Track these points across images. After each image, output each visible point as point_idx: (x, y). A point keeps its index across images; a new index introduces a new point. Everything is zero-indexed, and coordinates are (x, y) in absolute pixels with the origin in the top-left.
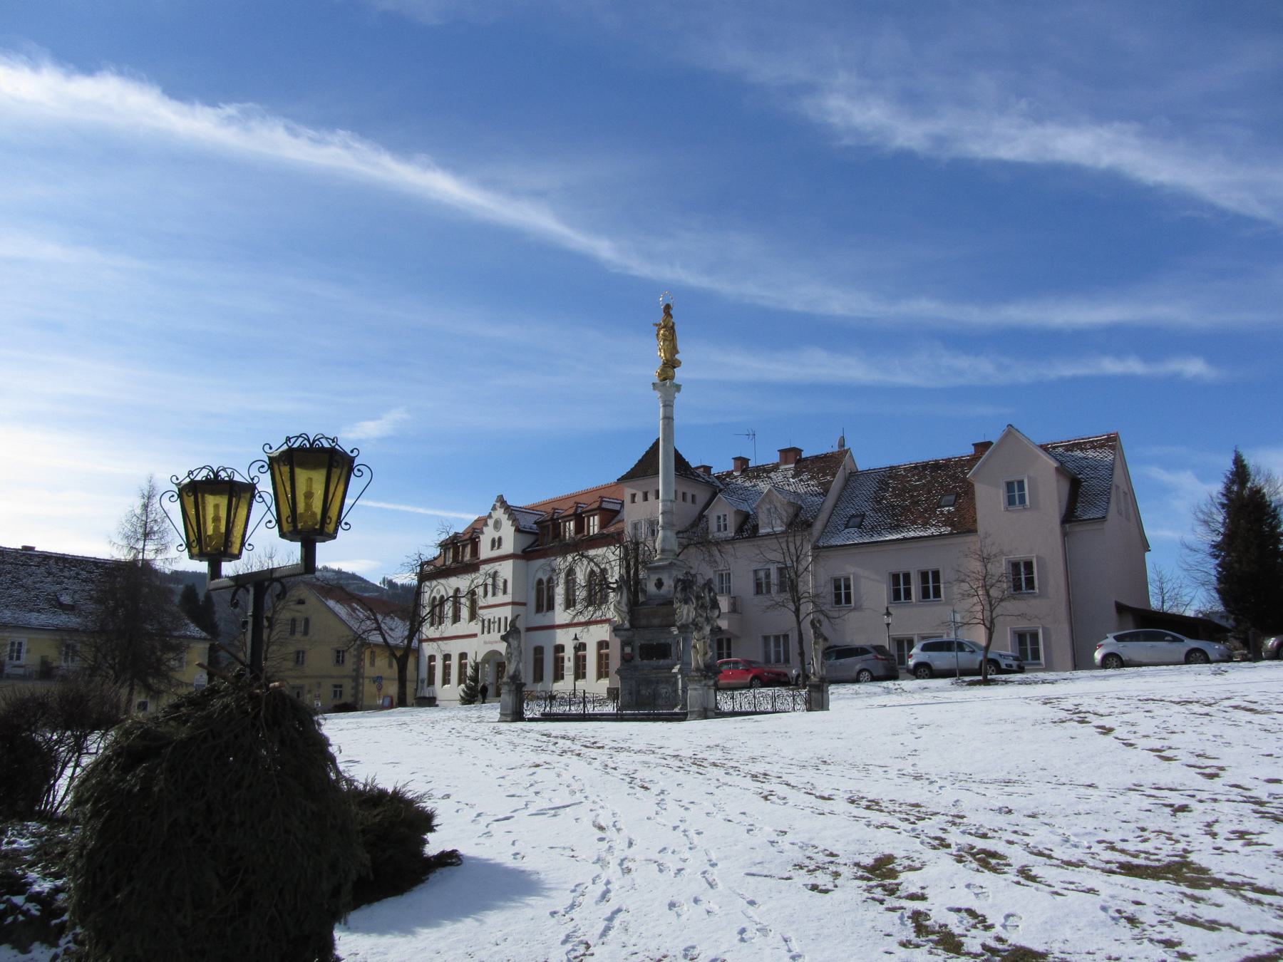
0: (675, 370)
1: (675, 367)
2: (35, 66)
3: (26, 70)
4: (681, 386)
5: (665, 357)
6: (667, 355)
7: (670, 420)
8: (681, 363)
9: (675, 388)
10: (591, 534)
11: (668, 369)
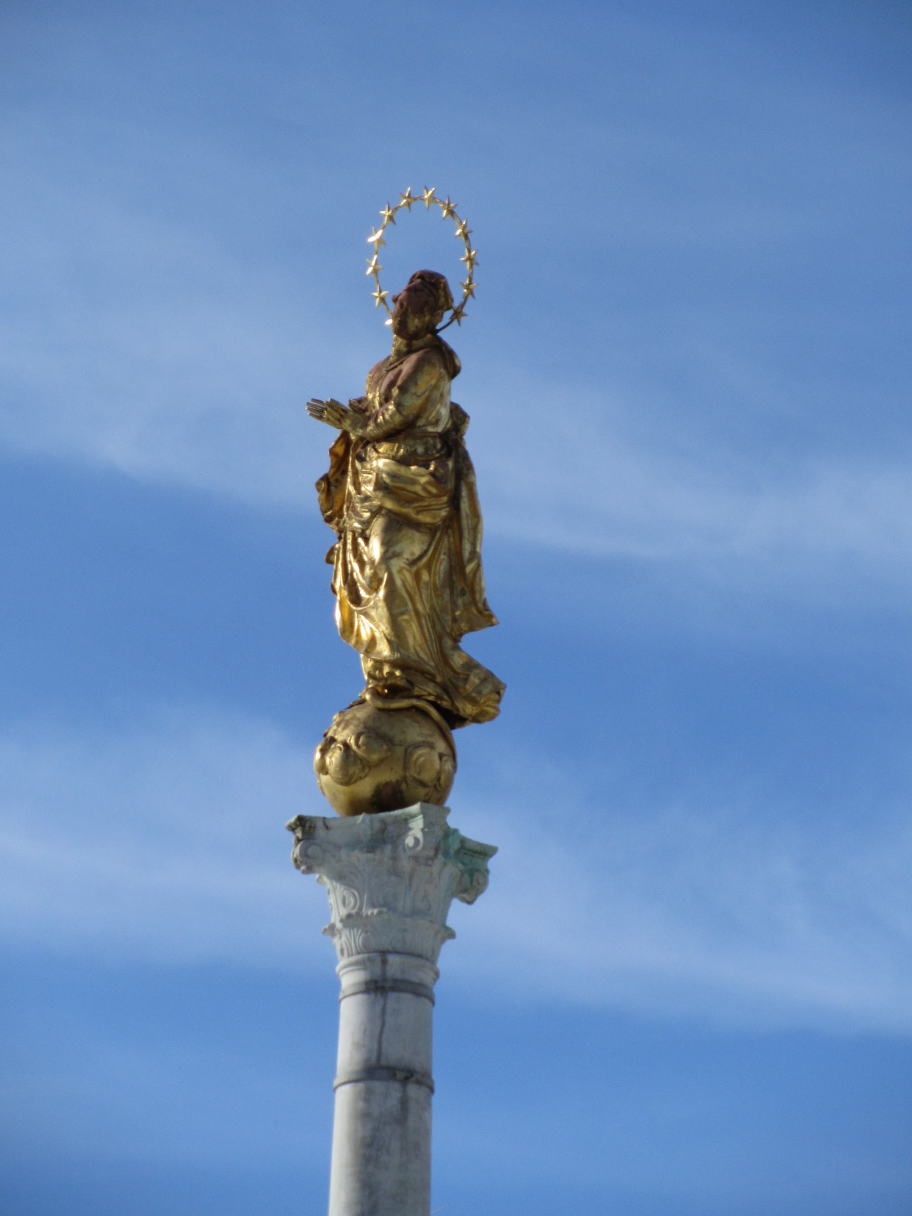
0: (457, 734)
1: (455, 720)
2: (467, 427)
3: (467, 425)
4: (486, 852)
5: (397, 639)
6: (414, 636)
7: (413, 1090)
8: (498, 692)
9: (452, 870)
10: (397, 444)
11: (415, 732)
